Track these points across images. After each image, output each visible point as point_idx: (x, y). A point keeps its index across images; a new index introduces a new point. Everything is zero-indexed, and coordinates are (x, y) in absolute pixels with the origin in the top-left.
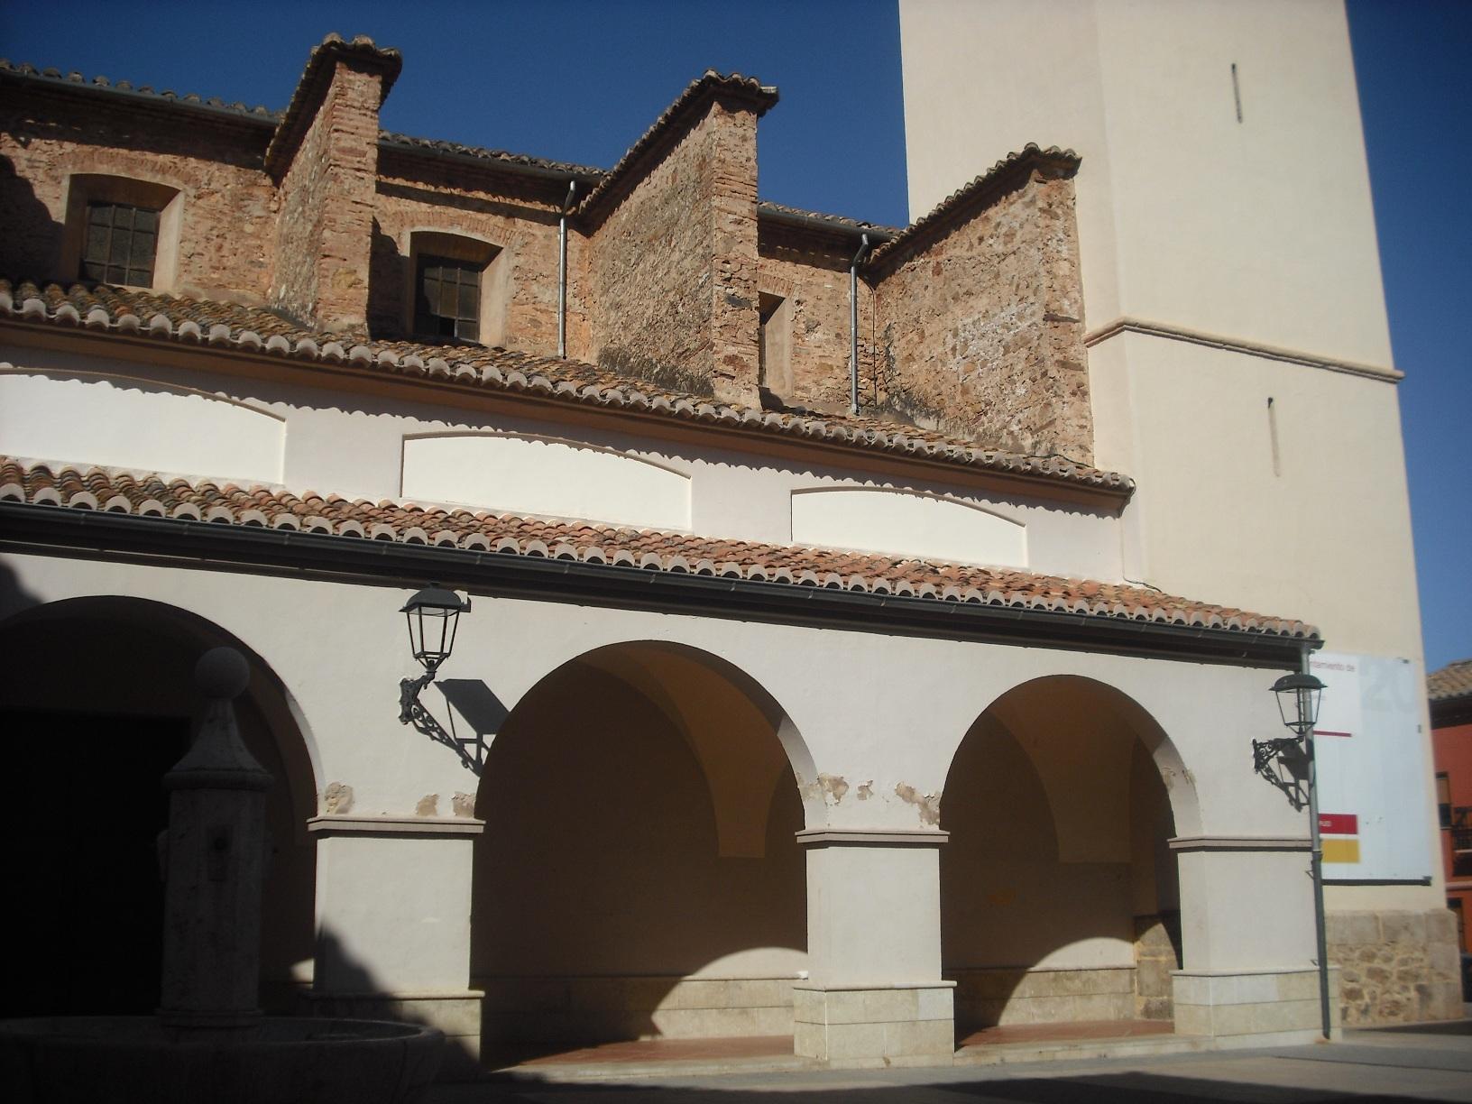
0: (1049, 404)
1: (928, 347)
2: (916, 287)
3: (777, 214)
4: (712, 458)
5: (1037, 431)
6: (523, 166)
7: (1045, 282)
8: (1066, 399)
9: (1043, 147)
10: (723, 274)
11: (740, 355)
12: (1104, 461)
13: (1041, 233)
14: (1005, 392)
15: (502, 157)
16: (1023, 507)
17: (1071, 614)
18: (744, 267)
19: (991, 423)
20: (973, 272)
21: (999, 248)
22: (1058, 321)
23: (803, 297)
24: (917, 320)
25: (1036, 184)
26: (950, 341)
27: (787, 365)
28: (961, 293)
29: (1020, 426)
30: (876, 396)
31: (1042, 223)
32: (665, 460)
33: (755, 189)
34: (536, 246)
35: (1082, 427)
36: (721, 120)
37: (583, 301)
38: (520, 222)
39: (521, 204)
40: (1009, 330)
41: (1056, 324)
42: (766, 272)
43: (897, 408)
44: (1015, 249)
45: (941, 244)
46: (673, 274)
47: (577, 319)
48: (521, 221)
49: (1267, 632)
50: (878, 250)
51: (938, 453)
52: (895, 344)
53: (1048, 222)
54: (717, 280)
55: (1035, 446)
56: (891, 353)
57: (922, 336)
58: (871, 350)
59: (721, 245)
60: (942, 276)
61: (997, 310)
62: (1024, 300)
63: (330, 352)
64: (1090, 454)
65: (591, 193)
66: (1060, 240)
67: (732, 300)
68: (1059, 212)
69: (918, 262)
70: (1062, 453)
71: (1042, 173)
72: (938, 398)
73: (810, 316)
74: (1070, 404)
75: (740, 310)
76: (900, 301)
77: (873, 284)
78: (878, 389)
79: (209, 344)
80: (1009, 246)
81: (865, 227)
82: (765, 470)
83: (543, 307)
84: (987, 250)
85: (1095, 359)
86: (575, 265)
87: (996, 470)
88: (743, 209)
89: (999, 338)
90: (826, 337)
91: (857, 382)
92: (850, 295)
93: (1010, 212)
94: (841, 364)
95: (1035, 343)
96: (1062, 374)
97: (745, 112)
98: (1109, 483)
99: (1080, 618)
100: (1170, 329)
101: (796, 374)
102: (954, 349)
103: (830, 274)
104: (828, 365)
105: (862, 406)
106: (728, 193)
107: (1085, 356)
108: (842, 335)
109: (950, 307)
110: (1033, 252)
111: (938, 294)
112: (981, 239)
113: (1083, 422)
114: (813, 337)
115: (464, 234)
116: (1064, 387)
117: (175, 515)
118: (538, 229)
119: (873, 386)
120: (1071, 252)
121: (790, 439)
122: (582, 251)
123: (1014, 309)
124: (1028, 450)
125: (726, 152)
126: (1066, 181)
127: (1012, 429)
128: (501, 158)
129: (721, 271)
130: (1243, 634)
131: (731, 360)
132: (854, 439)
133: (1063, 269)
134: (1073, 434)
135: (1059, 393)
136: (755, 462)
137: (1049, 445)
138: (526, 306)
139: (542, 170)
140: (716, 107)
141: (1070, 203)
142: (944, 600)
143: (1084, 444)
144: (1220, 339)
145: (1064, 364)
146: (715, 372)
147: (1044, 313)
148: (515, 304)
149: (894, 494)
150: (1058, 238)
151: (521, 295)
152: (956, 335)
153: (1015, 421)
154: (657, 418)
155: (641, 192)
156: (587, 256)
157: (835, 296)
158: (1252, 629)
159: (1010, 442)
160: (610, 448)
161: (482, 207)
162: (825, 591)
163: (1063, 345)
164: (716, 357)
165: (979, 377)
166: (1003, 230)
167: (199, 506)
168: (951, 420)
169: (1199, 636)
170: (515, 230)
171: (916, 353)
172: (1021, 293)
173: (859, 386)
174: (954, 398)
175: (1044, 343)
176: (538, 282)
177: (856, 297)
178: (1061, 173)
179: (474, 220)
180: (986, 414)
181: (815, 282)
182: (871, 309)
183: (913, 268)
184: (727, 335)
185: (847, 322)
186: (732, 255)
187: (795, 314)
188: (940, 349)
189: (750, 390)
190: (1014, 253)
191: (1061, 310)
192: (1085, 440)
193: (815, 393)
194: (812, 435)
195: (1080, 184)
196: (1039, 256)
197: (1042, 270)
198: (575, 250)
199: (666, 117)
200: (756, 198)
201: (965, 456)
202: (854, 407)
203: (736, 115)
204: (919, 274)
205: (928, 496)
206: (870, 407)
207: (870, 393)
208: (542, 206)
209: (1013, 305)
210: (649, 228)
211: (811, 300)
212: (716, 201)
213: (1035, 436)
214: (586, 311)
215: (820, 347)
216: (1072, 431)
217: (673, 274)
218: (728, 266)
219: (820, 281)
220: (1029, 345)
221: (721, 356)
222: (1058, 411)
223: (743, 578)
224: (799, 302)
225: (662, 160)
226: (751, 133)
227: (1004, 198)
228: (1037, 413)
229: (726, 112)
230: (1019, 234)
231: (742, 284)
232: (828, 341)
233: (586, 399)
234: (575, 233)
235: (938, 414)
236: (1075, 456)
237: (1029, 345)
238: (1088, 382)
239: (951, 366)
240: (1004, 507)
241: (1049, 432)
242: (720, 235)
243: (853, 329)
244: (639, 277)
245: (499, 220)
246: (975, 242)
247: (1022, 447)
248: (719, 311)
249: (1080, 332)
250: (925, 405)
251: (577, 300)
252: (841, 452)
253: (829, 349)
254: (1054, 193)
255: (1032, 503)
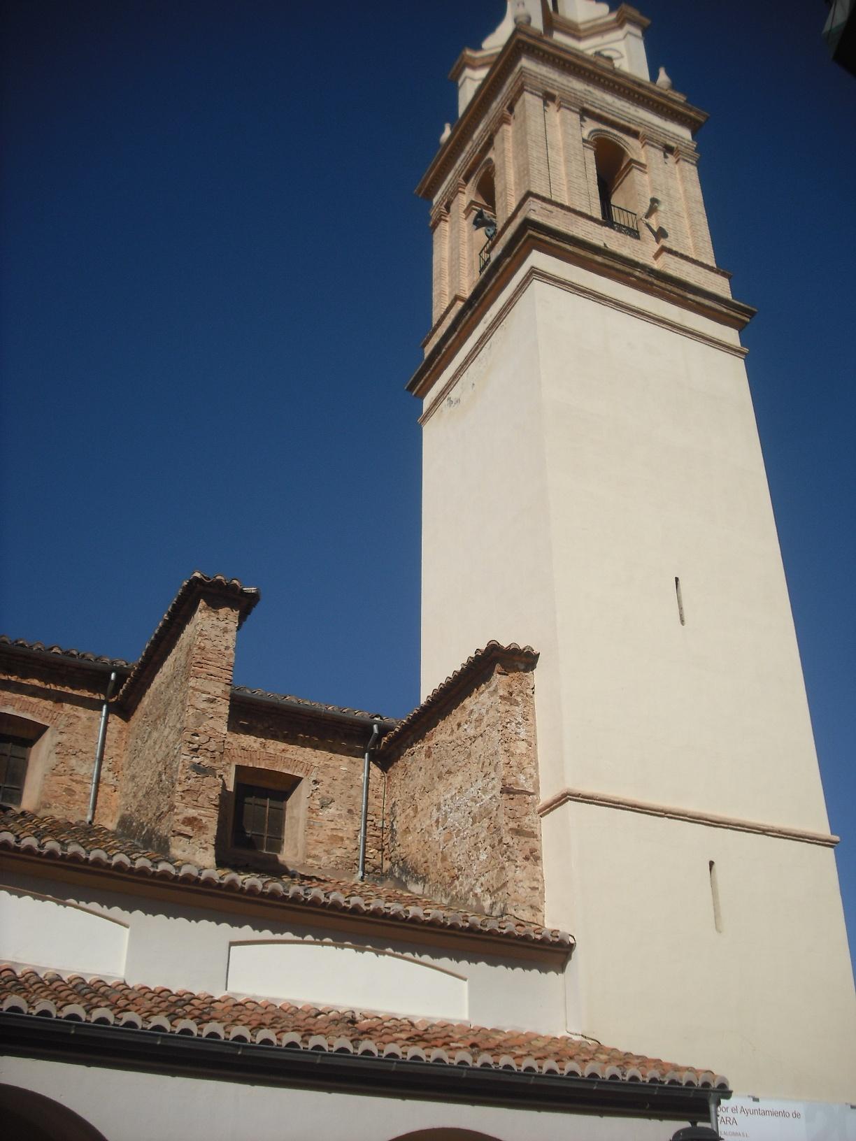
0: (503, 868)
1: (420, 820)
2: (413, 769)
3: (298, 706)
4: (151, 910)
5: (495, 892)
6: (71, 659)
7: (503, 759)
8: (519, 863)
9: (505, 644)
10: (191, 745)
11: (199, 817)
12: (553, 920)
13: (500, 717)
14: (472, 858)
15: (55, 650)
16: (464, 963)
17: (451, 1066)
18: (212, 740)
19: (462, 886)
20: (453, 753)
21: (471, 732)
22: (514, 793)
23: (320, 778)
24: (413, 797)
25: (498, 676)
26: (435, 815)
27: (300, 836)
28: (444, 772)
29: (482, 889)
30: (382, 864)
31: (502, 708)
32: (104, 910)
33: (231, 673)
34: (79, 727)
35: (534, 889)
36: (205, 615)
37: (116, 774)
38: (67, 707)
39: (70, 691)
40: (476, 802)
41: (511, 796)
42: (288, 756)
43: (397, 875)
44: (482, 732)
45: (432, 731)
46: (163, 748)
47: (108, 790)
48: (68, 705)
49: (670, 1083)
50: (386, 738)
51: (374, 909)
52: (398, 819)
53: (507, 708)
54: (185, 750)
55: (493, 905)
56: (395, 827)
57: (416, 810)
58: (379, 825)
59: (192, 720)
60: (431, 759)
61: (468, 786)
62: (487, 776)
63: (142, 865)
64: (540, 913)
65: (389, 738)
66: (519, 723)
67: (197, 768)
68: (519, 699)
69: (416, 747)
70: (513, 912)
71: (503, 667)
72: (425, 865)
73: (325, 794)
74: (522, 867)
75: (204, 777)
76: (402, 782)
77: (384, 768)
78: (384, 858)
79: (89, 862)
80: (478, 730)
81: (377, 719)
82: (204, 923)
83: (78, 778)
84: (463, 734)
85: (547, 827)
86: (113, 743)
87: (434, 926)
88: (216, 689)
89: (469, 809)
90: (339, 812)
91: (364, 852)
92: (363, 776)
93: (480, 702)
94: (351, 835)
95: (494, 814)
96: (516, 840)
97: (228, 609)
98: (548, 940)
99: (461, 1070)
100: (612, 799)
101: (309, 844)
102: (437, 821)
103: (346, 759)
104: (339, 837)
105: (368, 873)
106: (204, 676)
107: (539, 824)
108: (354, 811)
109: (436, 785)
110: (495, 733)
111: (428, 774)
112: (459, 725)
113: (535, 884)
114: (326, 813)
115: (15, 713)
116: (517, 853)
117: (63, 1014)
118: (82, 713)
119: (380, 856)
120: (528, 734)
121: (228, 894)
122: (120, 732)
123: (480, 784)
124: (487, 911)
125: (205, 641)
126: (527, 674)
127: (476, 892)
128: (53, 651)
129: (190, 742)
130: (644, 1086)
131: (190, 821)
132: (290, 895)
133: (521, 747)
134: (524, 895)
135: (512, 857)
136: (194, 914)
137: (502, 906)
138: (63, 777)
139: (89, 663)
140: (202, 603)
141: (529, 692)
142: (309, 1050)
143: (535, 904)
144: (661, 808)
145: (518, 832)
146: (174, 831)
147: (501, 786)
148: (54, 775)
149: (320, 947)
150: (517, 722)
151: (59, 768)
152: (439, 809)
153: (478, 884)
154: (96, 869)
155: (159, 679)
156: (124, 737)
157: (349, 777)
158: (653, 1080)
159: (474, 903)
160: (369, 947)
161: (35, 692)
162: (177, 1038)
163: (518, 814)
164: (176, 818)
165: (454, 846)
166: (475, 716)
167: (111, 1010)
168: (433, 885)
169: (595, 1088)
170: (62, 712)
171: (412, 826)
172: (485, 770)
173: (367, 856)
174: (436, 865)
175: (501, 812)
176: (78, 757)
177: (368, 778)
178: (522, 666)
179: (26, 702)
180: (458, 878)
181: (331, 765)
182: (381, 789)
183: (412, 753)
184: (188, 799)
185: (359, 800)
186: (202, 729)
187: (311, 792)
188: (428, 822)
189: (206, 849)
190: (481, 735)
191: (517, 784)
192: (536, 900)
193: (324, 860)
194: (292, 898)
195: (538, 676)
196: (497, 737)
197: (500, 750)
198: (114, 731)
199: (169, 614)
200: (231, 681)
201: (402, 913)
202: (360, 874)
203: (220, 610)
204: (416, 759)
205: (369, 950)
206: (376, 874)
207: (377, 862)
208: (89, 693)
209: (479, 782)
210: (157, 710)
211: (327, 780)
212: (192, 682)
213: (493, 898)
214: (117, 783)
215: (332, 821)
216: (524, 891)
217: (163, 748)
218: (197, 738)
219: (337, 764)
220: (490, 816)
221: (180, 817)
222: (511, 874)
223: (278, 1045)
224: (316, 782)
225: (170, 651)
226: (233, 626)
227: (476, 690)
228: (494, 876)
229: (210, 608)
230: (485, 719)
231: (209, 754)
232: (340, 816)
233: (48, 853)
234: (116, 717)
235: (424, 880)
236: (526, 915)
237: (490, 816)
238: (541, 847)
239: (435, 836)
240: (445, 962)
241: (502, 893)
242: (191, 711)
243: (364, 806)
244: (147, 752)
245: (49, 704)
246: (455, 727)
247: (483, 908)
248: (183, 777)
249: (534, 803)
250: (416, 872)
251: (111, 774)
252: (277, 906)
253: (341, 822)
254: (514, 683)
255: (474, 959)
